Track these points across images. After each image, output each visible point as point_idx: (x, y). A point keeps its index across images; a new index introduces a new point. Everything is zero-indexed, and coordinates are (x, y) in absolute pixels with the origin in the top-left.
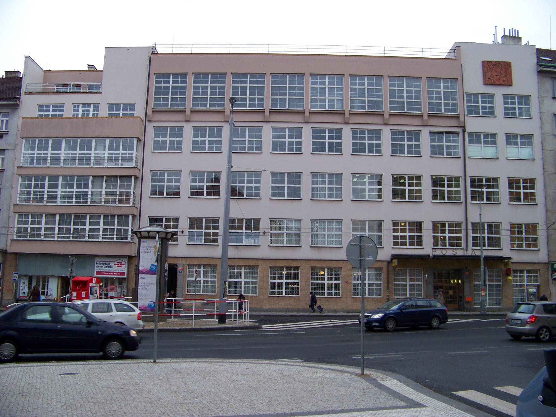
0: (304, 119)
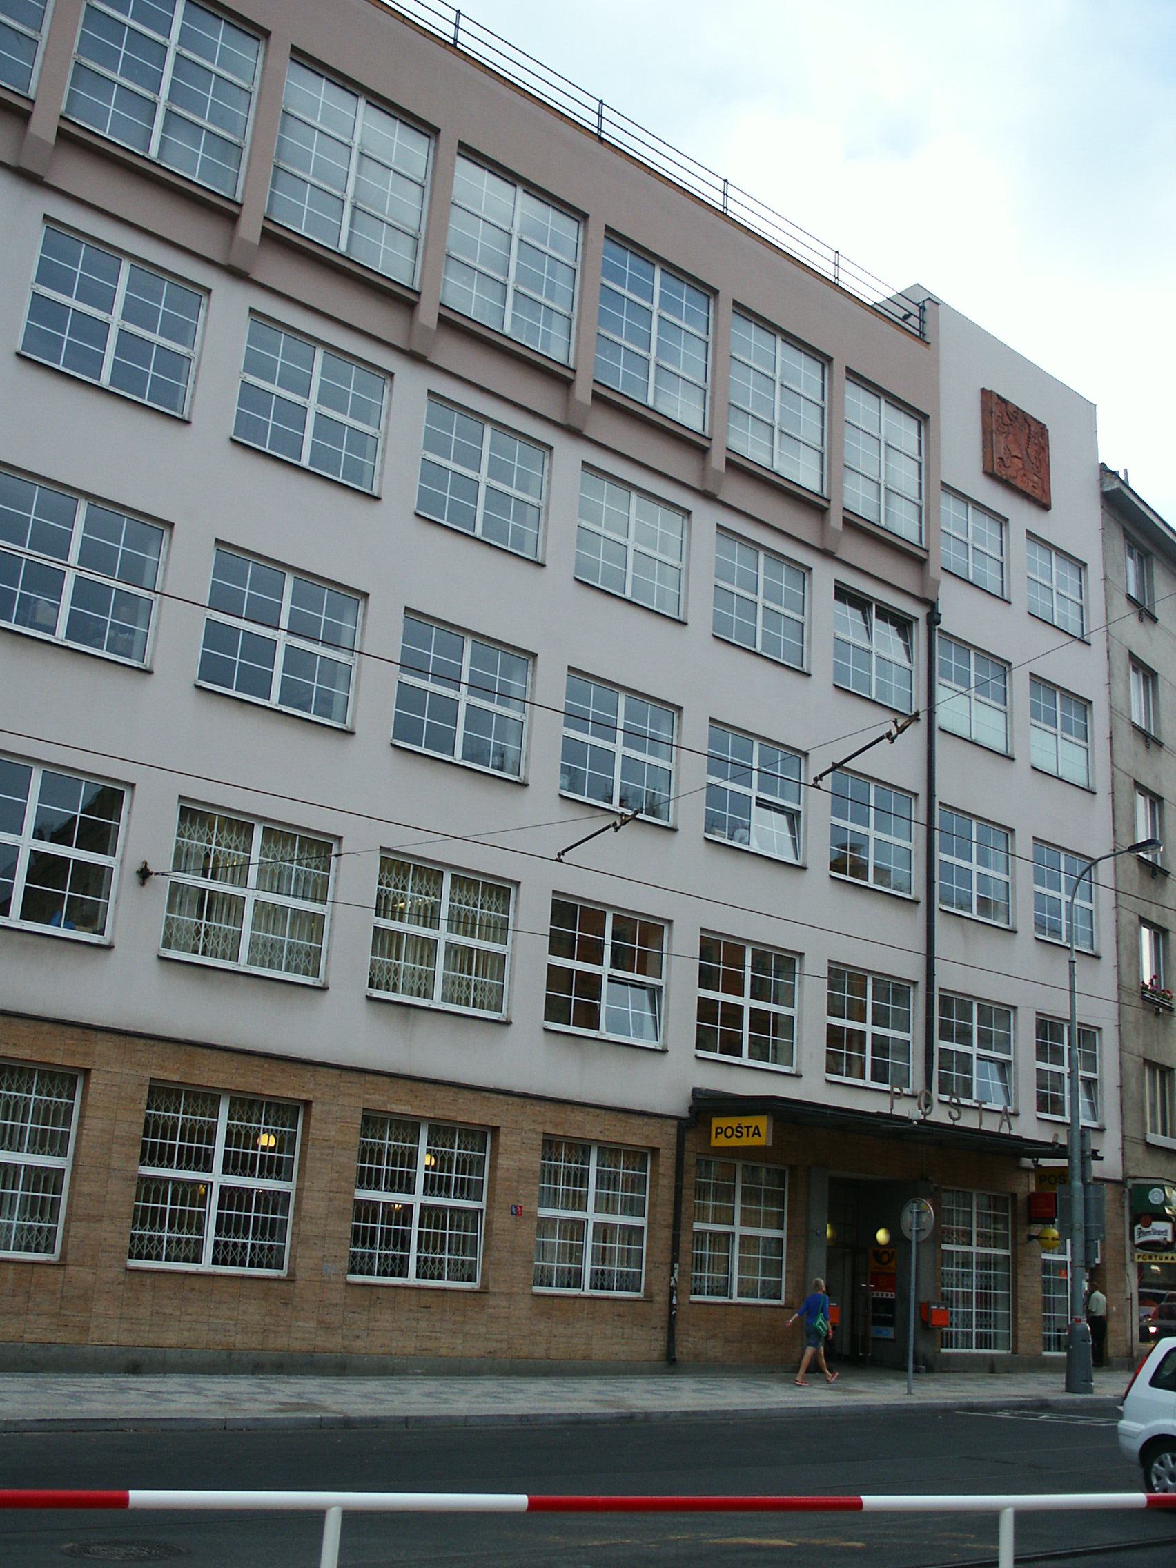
0: (409, 337)
